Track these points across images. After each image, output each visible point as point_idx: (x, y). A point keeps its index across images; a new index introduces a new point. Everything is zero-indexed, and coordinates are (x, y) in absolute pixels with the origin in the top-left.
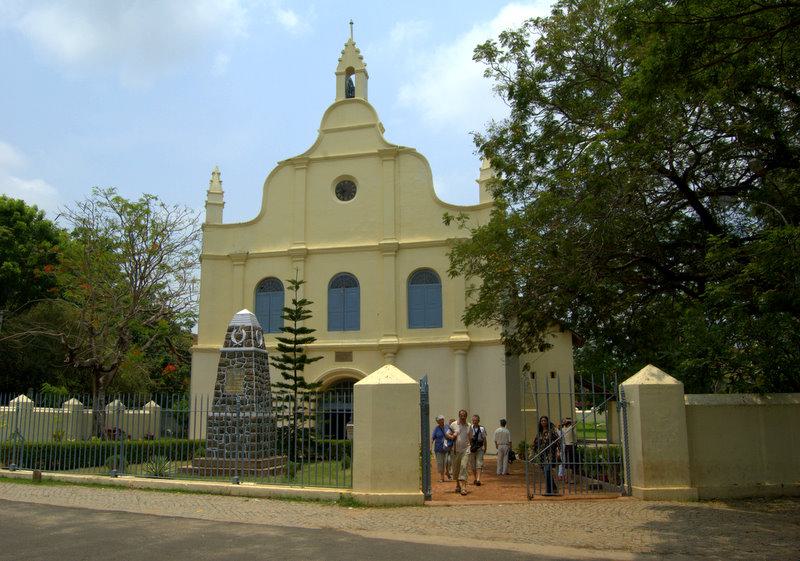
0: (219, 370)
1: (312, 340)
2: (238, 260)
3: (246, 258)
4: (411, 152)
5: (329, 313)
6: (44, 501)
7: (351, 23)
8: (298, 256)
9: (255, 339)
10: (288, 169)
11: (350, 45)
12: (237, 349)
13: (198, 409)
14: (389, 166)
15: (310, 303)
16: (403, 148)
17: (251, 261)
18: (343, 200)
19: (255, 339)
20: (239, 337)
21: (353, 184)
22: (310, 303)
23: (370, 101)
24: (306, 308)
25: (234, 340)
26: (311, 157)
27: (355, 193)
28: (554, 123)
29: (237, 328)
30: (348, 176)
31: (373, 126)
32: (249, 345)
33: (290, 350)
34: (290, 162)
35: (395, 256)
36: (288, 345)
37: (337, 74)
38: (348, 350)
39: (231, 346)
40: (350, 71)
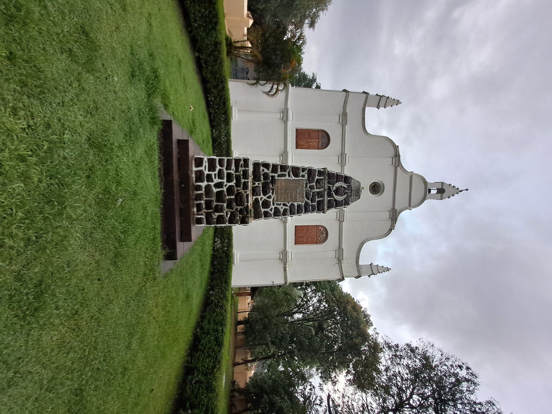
4: (391, 230)
7: (467, 190)
14: (387, 215)
16: (395, 223)
34: (397, 155)
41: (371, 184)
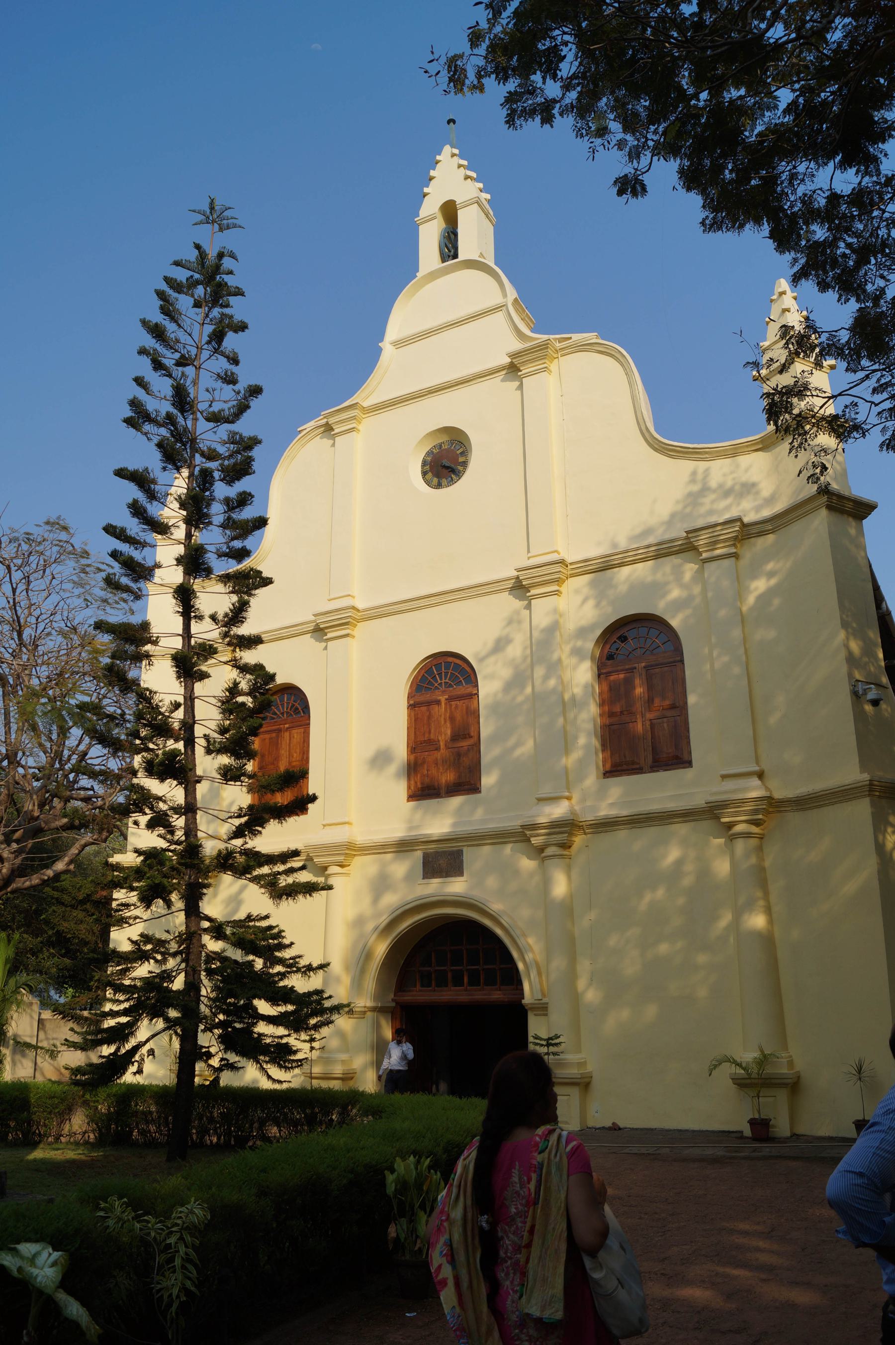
41: (428, 483)
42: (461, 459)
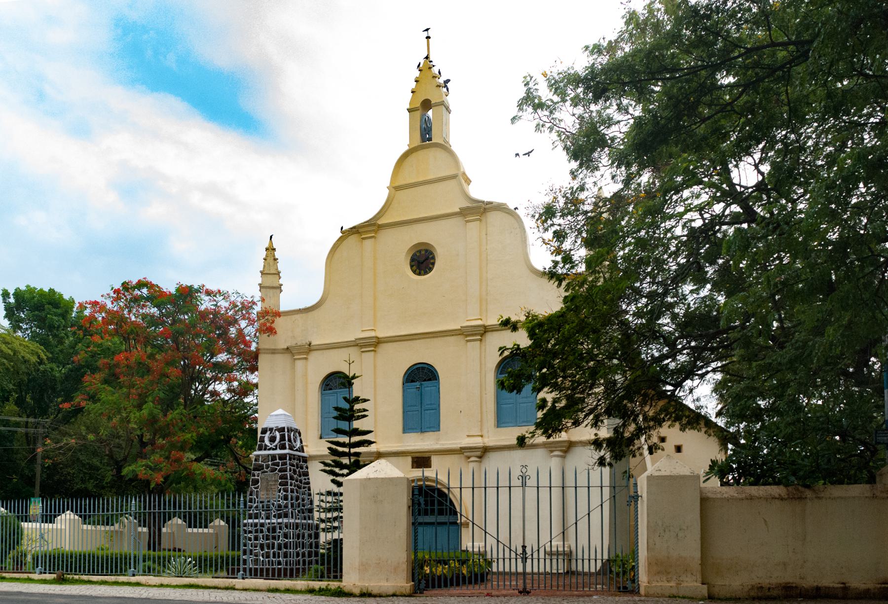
0: (309, 479)
1: (370, 443)
2: (300, 353)
3: (310, 348)
4: (501, 208)
5: (405, 412)
6: (60, 593)
8: (365, 346)
9: (290, 440)
10: (353, 239)
11: (426, 67)
12: (271, 452)
13: (586, 556)
14: (474, 227)
15: (365, 400)
16: (491, 203)
17: (382, 345)
18: (419, 274)
19: (290, 440)
20: (272, 440)
21: (432, 253)
22: (365, 400)
23: (454, 148)
24: (357, 407)
25: (267, 442)
26: (380, 222)
27: (433, 264)
28: (695, 152)
29: (271, 429)
30: (433, 246)
31: (454, 177)
32: (283, 447)
33: (343, 454)
34: (355, 230)
35: (481, 340)
36: (340, 449)
37: (409, 110)
38: (426, 455)
39: (265, 449)
40: (427, 105)
42: (432, 261)
